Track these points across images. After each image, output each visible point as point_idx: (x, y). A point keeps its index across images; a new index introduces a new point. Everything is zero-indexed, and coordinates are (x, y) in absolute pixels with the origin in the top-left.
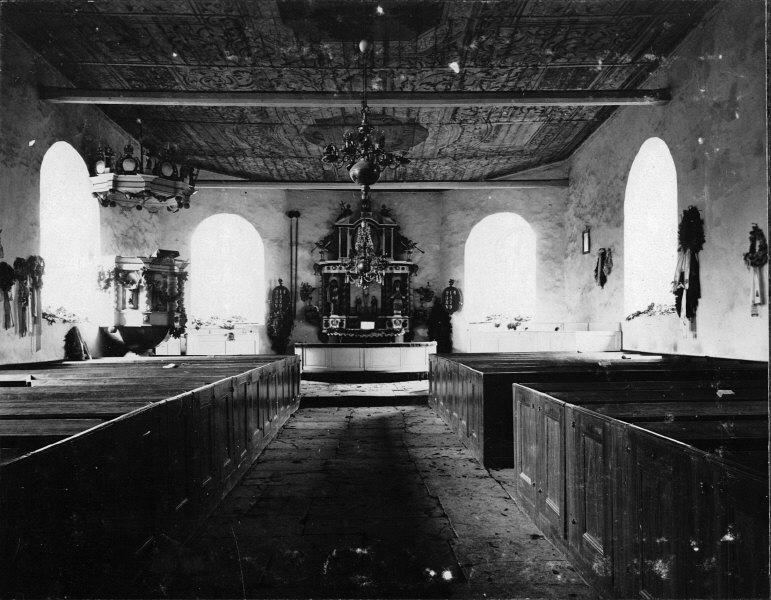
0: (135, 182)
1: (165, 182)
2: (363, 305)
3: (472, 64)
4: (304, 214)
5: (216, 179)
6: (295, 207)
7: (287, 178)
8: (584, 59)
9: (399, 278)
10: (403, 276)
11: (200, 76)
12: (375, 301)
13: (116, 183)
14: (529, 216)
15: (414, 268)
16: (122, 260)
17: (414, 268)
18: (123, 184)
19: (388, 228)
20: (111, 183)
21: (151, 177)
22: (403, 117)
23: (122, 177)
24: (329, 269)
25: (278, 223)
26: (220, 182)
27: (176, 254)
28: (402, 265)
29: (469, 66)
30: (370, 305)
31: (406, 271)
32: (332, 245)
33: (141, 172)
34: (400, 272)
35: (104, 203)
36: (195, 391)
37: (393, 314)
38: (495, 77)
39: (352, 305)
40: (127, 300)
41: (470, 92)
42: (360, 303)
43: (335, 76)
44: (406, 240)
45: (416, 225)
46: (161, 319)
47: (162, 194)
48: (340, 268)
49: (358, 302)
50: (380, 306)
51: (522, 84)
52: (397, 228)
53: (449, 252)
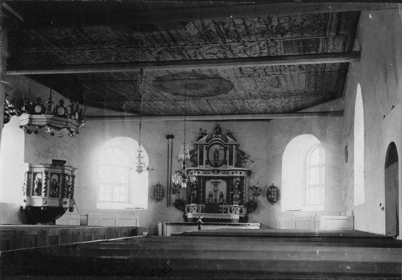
0: (41, 119)
1: (58, 118)
2: (214, 198)
3: (231, 41)
4: (176, 137)
5: (113, 114)
6: (171, 132)
7: (163, 114)
8: (302, 34)
9: (238, 179)
10: (242, 178)
11: (73, 56)
12: (222, 196)
13: (31, 119)
14: (322, 137)
15: (249, 173)
16: (33, 166)
17: (249, 173)
18: (36, 120)
19: (231, 145)
20: (28, 120)
21: (50, 116)
22: (208, 74)
23: (34, 116)
24: (233, 173)
25: (161, 144)
26: (103, 117)
27: (65, 162)
28: (240, 170)
29: (229, 42)
30: (218, 198)
31: (243, 174)
32: (196, 158)
33: (44, 113)
34: (238, 175)
35: (28, 132)
36: (114, 257)
37: (233, 204)
38: (251, 48)
39: (207, 197)
40: (35, 190)
41: (240, 58)
42: (212, 196)
43: (150, 52)
44: (243, 153)
45: (249, 140)
46: (55, 203)
47: (59, 126)
48: (241, 173)
49: (211, 196)
50: (225, 197)
51: (272, 51)
52: (237, 145)
53: (273, 162)
